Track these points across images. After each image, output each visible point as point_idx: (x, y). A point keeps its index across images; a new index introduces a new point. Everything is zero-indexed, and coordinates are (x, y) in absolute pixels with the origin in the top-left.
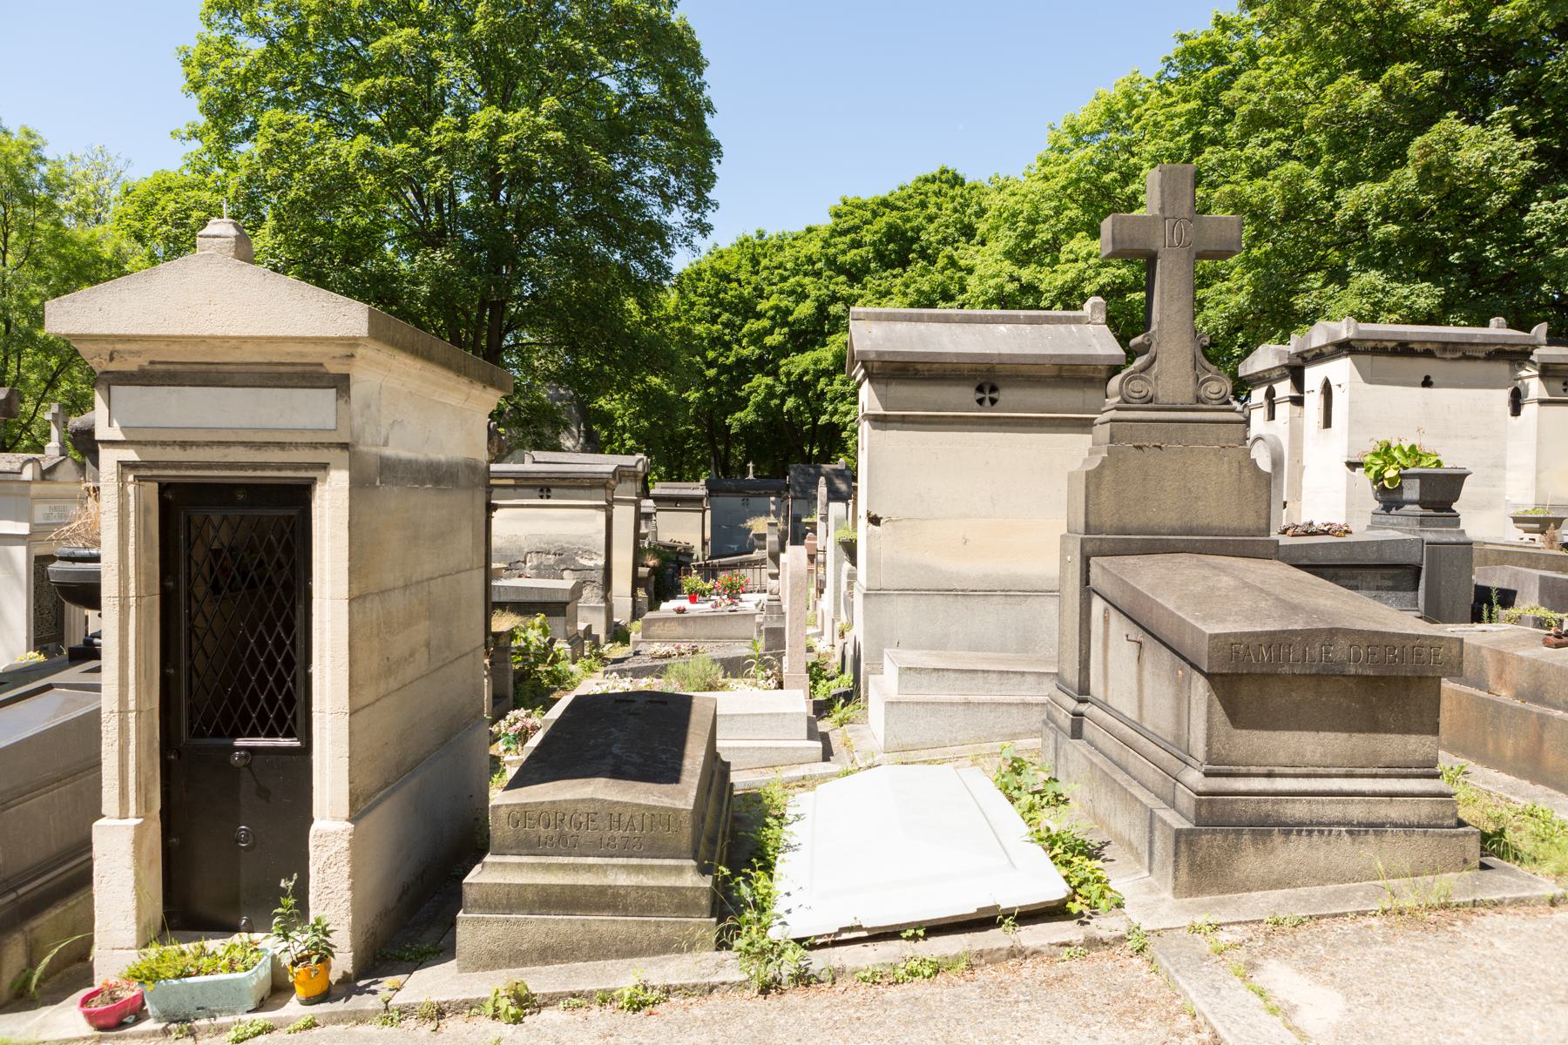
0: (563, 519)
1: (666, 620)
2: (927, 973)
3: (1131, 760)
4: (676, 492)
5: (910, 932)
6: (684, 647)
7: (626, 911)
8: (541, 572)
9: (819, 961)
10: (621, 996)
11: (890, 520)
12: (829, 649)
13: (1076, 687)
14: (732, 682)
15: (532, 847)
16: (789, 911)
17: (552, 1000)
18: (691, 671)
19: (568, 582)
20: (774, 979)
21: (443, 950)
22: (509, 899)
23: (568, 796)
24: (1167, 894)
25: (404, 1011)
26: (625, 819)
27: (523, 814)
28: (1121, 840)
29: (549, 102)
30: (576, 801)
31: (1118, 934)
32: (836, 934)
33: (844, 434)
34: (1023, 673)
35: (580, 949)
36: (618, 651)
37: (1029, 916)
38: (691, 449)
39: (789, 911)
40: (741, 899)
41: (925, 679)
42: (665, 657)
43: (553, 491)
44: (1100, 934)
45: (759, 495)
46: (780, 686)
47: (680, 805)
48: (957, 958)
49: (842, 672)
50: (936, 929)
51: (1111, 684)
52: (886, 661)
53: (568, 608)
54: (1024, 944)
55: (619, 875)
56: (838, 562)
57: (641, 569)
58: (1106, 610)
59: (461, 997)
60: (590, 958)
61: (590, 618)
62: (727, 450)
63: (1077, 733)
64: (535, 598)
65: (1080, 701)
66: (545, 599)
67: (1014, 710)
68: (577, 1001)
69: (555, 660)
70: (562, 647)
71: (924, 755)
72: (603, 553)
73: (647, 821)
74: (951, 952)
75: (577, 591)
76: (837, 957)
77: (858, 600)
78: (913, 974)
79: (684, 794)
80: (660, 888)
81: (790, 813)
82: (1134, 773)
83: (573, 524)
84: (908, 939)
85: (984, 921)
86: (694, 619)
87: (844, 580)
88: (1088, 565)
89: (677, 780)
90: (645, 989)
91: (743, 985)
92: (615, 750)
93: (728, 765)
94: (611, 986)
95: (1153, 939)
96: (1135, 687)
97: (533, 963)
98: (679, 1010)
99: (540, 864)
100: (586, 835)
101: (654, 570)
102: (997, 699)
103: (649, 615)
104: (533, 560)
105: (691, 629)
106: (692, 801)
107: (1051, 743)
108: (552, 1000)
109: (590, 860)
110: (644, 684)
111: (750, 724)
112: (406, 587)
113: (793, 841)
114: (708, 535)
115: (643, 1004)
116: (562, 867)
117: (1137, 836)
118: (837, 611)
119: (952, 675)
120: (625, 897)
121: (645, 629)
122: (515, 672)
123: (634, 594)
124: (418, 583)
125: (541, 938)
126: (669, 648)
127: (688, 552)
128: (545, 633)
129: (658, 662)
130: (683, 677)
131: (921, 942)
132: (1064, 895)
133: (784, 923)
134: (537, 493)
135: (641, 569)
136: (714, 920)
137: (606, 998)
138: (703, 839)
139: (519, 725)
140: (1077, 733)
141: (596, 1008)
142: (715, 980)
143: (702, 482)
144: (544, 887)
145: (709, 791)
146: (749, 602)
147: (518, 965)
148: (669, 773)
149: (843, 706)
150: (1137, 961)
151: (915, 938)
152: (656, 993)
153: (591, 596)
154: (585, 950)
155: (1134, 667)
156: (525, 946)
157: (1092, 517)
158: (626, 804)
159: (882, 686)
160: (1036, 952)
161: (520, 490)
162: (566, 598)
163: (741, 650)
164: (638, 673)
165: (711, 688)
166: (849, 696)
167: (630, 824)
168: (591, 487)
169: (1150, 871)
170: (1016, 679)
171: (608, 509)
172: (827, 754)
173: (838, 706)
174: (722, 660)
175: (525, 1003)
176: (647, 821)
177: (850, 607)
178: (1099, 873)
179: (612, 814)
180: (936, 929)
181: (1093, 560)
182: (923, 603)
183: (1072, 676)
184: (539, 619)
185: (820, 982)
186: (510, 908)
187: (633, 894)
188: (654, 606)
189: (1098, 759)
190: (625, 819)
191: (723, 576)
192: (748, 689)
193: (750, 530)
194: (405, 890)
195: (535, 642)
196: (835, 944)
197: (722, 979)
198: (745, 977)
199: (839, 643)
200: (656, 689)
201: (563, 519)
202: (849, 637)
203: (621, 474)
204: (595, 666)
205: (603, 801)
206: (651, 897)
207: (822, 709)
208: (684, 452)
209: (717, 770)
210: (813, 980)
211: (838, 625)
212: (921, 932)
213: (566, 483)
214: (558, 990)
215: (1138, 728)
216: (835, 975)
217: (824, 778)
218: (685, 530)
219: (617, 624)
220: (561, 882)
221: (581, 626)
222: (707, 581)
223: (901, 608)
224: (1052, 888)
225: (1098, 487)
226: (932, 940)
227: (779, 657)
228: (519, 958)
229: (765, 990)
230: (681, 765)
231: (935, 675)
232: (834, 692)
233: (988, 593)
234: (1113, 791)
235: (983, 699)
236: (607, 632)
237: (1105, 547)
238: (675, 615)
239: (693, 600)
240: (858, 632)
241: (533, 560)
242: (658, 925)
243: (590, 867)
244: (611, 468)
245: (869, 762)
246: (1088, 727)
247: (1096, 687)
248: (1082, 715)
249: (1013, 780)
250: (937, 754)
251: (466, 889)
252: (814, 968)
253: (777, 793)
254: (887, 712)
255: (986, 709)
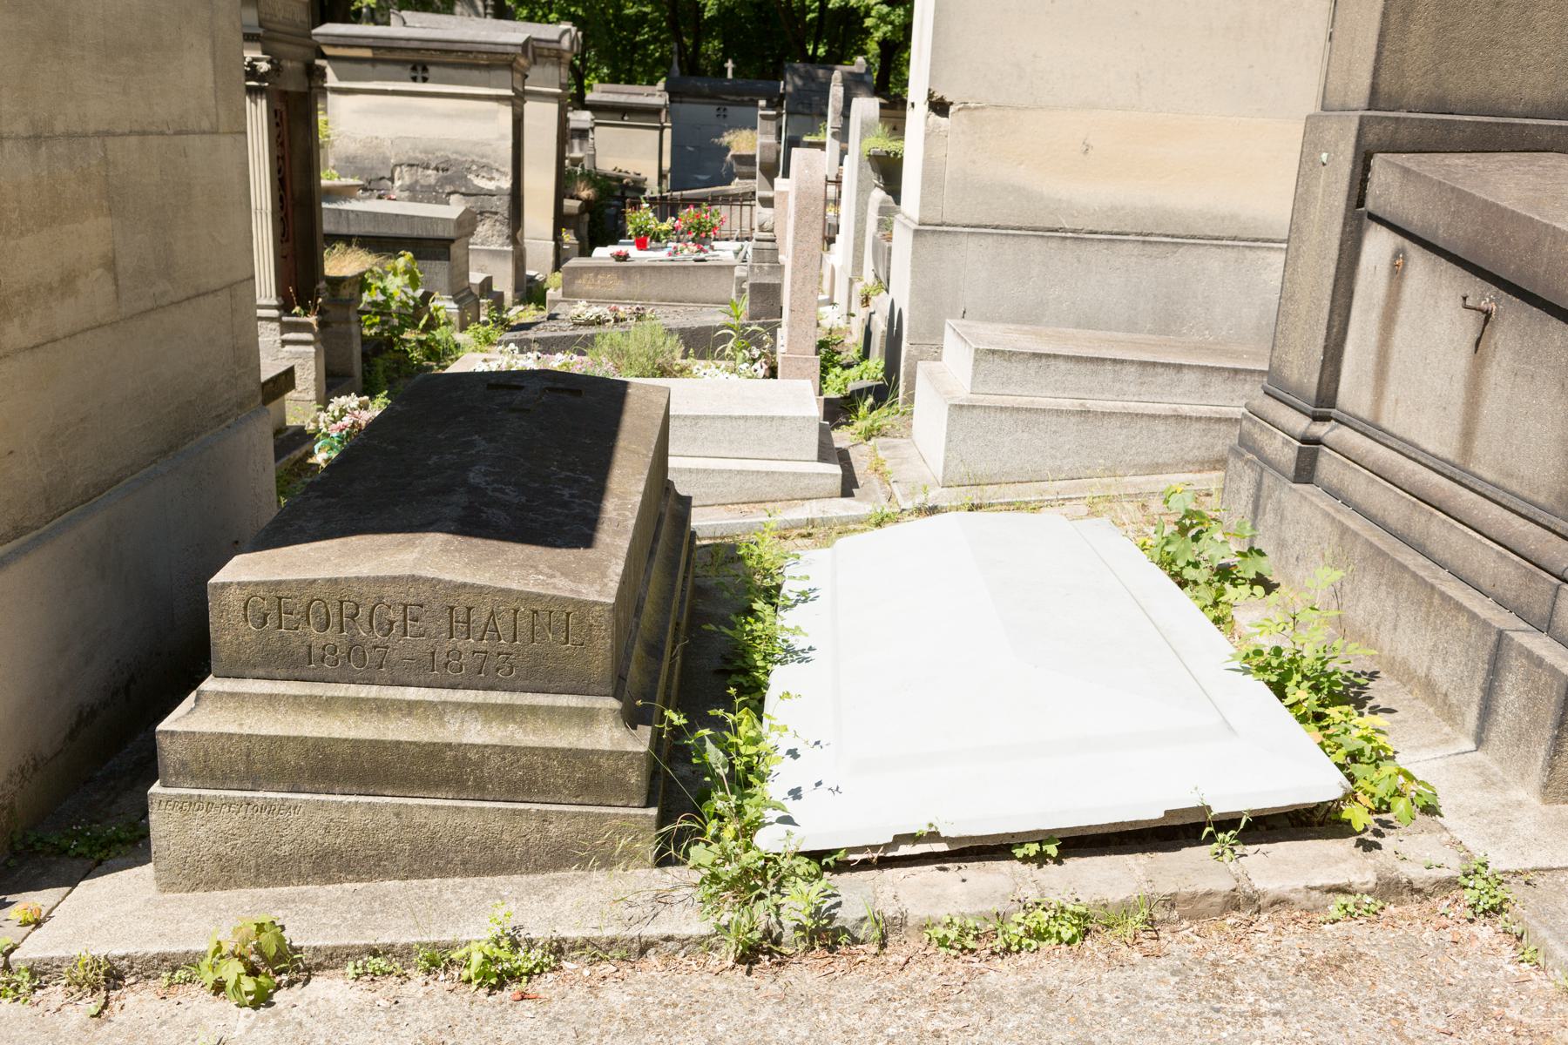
0: (447, 115)
1: (599, 270)
2: (1066, 935)
3: (1434, 528)
4: (622, 99)
5: (1033, 849)
6: (623, 311)
7: (480, 790)
8: (415, 192)
9: (858, 896)
10: (465, 963)
11: (965, 107)
12: (842, 324)
13: (1313, 392)
14: (697, 365)
15: (295, 664)
16: (796, 794)
17: (333, 959)
18: (633, 347)
19: (454, 209)
20: (768, 933)
21: (125, 843)
22: (250, 763)
23: (366, 569)
24: (1526, 793)
25: (40, 974)
26: (480, 617)
27: (275, 602)
28: (1406, 675)
29: (748, 628)
30: (378, 580)
31: (1444, 874)
32: (887, 846)
33: (868, 22)
34: (1179, 367)
35: (392, 857)
36: (529, 314)
37: (1267, 827)
38: (646, 42)
39: (796, 794)
40: (706, 769)
41: (1017, 369)
42: (589, 323)
43: (432, 70)
44: (1413, 871)
45: (742, 104)
46: (773, 373)
47: (589, 593)
48: (1127, 909)
49: (866, 355)
50: (1080, 843)
51: (1392, 390)
52: (950, 341)
53: (453, 248)
54: (1259, 885)
55: (469, 725)
56: (863, 192)
57: (568, 203)
58: (1398, 253)
59: (154, 949)
60: (411, 874)
61: (487, 263)
62: (696, 46)
63: (1305, 471)
64: (403, 231)
65: (1316, 418)
66: (418, 232)
67: (1160, 427)
68: (381, 962)
69: (432, 324)
70: (444, 306)
71: (1010, 493)
72: (508, 169)
73: (523, 624)
74: (1115, 895)
75: (467, 224)
76: (888, 892)
77: (902, 242)
78: (1040, 935)
79: (601, 570)
80: (547, 752)
81: (790, 589)
82: (1439, 556)
83: (462, 124)
84: (1026, 859)
85: (1176, 833)
86: (642, 269)
87: (873, 217)
88: (1367, 168)
89: (585, 539)
90: (515, 945)
91: (705, 944)
92: (474, 477)
93: (686, 502)
94: (447, 938)
95: (1515, 891)
96: (1457, 393)
97: (303, 879)
98: (579, 991)
99: (311, 699)
100: (402, 646)
101: (587, 205)
102: (1134, 407)
103: (575, 262)
104: (403, 178)
105: (638, 286)
106: (613, 585)
107: (1246, 486)
108: (333, 959)
109: (412, 693)
110: (556, 362)
111: (724, 434)
112: (36, 138)
113: (799, 643)
114: (667, 164)
115: (510, 976)
116: (356, 704)
117: (1455, 671)
118: (858, 265)
119: (1062, 365)
120: (479, 765)
121: (567, 283)
122: (365, 341)
123: (557, 237)
124: (70, 136)
125: (315, 837)
126: (592, 312)
127: (638, 187)
128: (414, 282)
129: (583, 331)
130: (619, 353)
131: (1051, 867)
132: (1338, 794)
133: (786, 820)
134: (408, 72)
135: (568, 203)
136: (653, 811)
137: (438, 960)
138: (638, 650)
139: (347, 420)
140: (1305, 471)
141: (418, 977)
142: (652, 931)
143: (661, 85)
144: (318, 743)
145: (652, 553)
146: (724, 252)
147: (273, 882)
148: (576, 528)
149: (872, 408)
150: (1484, 932)
151: (1041, 859)
152: (536, 954)
153: (490, 236)
154: (403, 860)
155: (1461, 361)
156: (286, 848)
157: (1385, 75)
158: (480, 590)
159: (942, 378)
160: (1279, 902)
161: (380, 67)
162: (449, 233)
163: (713, 317)
164: (548, 346)
165: (664, 372)
166: (882, 393)
167: (491, 628)
168: (489, 67)
169: (1480, 741)
170: (1166, 376)
171: (517, 102)
172: (848, 486)
173: (863, 410)
174: (682, 331)
175: (274, 967)
176: (523, 624)
177: (884, 255)
178: (1381, 739)
179: (457, 607)
180: (1080, 843)
181: (1378, 161)
182: (1010, 248)
183: (1304, 371)
184: (404, 260)
185: (855, 941)
186: (254, 780)
187: (495, 761)
188: (585, 251)
189: (1356, 523)
190: (480, 617)
191: (687, 214)
192: (722, 376)
193: (728, 149)
194: (84, 718)
195: (398, 295)
196: (885, 863)
197: (666, 930)
198: (705, 928)
199: (861, 313)
200: (576, 371)
201: (447, 115)
202: (881, 304)
203: (534, 51)
204: (495, 337)
205: (434, 583)
206: (531, 767)
207: (838, 411)
208: (635, 46)
209: (667, 508)
210: (844, 939)
211: (859, 287)
212: (1052, 850)
213: (451, 58)
214: (344, 942)
215: (1456, 474)
216: (887, 931)
217: (845, 527)
218: (634, 153)
219: (532, 279)
220: (352, 734)
221: (476, 278)
222: (663, 220)
223: (973, 257)
224: (1310, 778)
225: (1406, 15)
226: (1072, 863)
227: (773, 330)
228: (273, 869)
229: (749, 956)
230: (598, 509)
231: (1033, 364)
232: (852, 386)
233: (1115, 237)
234: (1394, 584)
235: (1110, 406)
236: (517, 289)
237: (1404, 135)
238: (613, 263)
239: (641, 245)
240: (901, 292)
241: (403, 178)
242: (544, 818)
243: (411, 707)
244: (519, 38)
245: (919, 500)
246: (1328, 465)
247: (1353, 392)
248: (1318, 442)
249: (1184, 550)
250: (1030, 493)
251: (164, 743)
252: (847, 915)
253: (767, 551)
254: (952, 421)
255: (1116, 422)
